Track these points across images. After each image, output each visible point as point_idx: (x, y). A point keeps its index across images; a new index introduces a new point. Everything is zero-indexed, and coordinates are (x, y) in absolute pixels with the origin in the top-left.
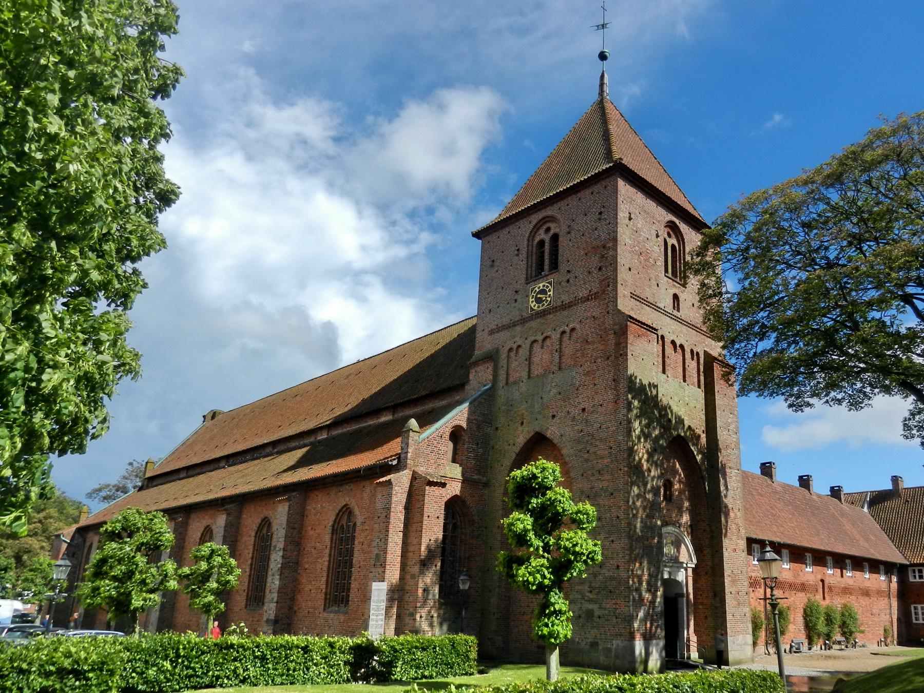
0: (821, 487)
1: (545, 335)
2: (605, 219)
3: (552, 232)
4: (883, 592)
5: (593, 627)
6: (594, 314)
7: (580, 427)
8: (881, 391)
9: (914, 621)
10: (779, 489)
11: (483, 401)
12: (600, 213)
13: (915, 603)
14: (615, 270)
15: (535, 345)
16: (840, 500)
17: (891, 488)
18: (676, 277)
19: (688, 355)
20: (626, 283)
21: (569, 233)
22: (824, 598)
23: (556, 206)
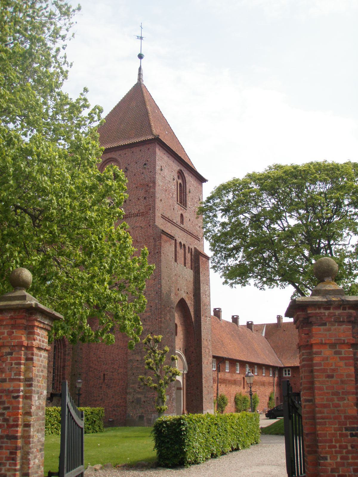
0: (242, 322)
2: (148, 169)
4: (271, 383)
5: (140, 407)
8: (289, 284)
12: (145, 164)
14: (154, 201)
16: (251, 329)
17: (276, 322)
19: (187, 251)
20: (160, 208)
22: (244, 388)
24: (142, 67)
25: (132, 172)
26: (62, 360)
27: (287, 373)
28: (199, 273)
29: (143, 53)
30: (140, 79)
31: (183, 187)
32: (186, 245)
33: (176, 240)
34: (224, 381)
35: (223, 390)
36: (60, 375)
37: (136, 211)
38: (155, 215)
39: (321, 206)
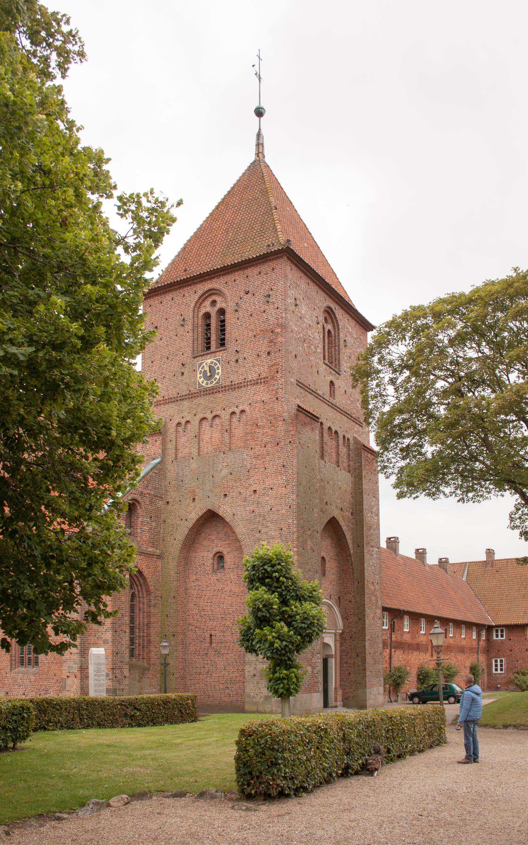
0: (432, 560)
1: (214, 413)
2: (273, 303)
4: (474, 648)
6: (264, 399)
9: (494, 672)
10: (401, 561)
11: (154, 475)
13: (496, 657)
15: (204, 422)
17: (485, 559)
18: (331, 363)
19: (341, 441)
21: (237, 311)
23: (223, 280)
24: (263, 132)
25: (247, 310)
26: (145, 614)
27: (499, 634)
28: (361, 479)
29: (263, 105)
31: (335, 337)
32: (339, 432)
33: (321, 423)
34: (401, 646)
35: (399, 658)
36: (143, 636)
37: (255, 376)
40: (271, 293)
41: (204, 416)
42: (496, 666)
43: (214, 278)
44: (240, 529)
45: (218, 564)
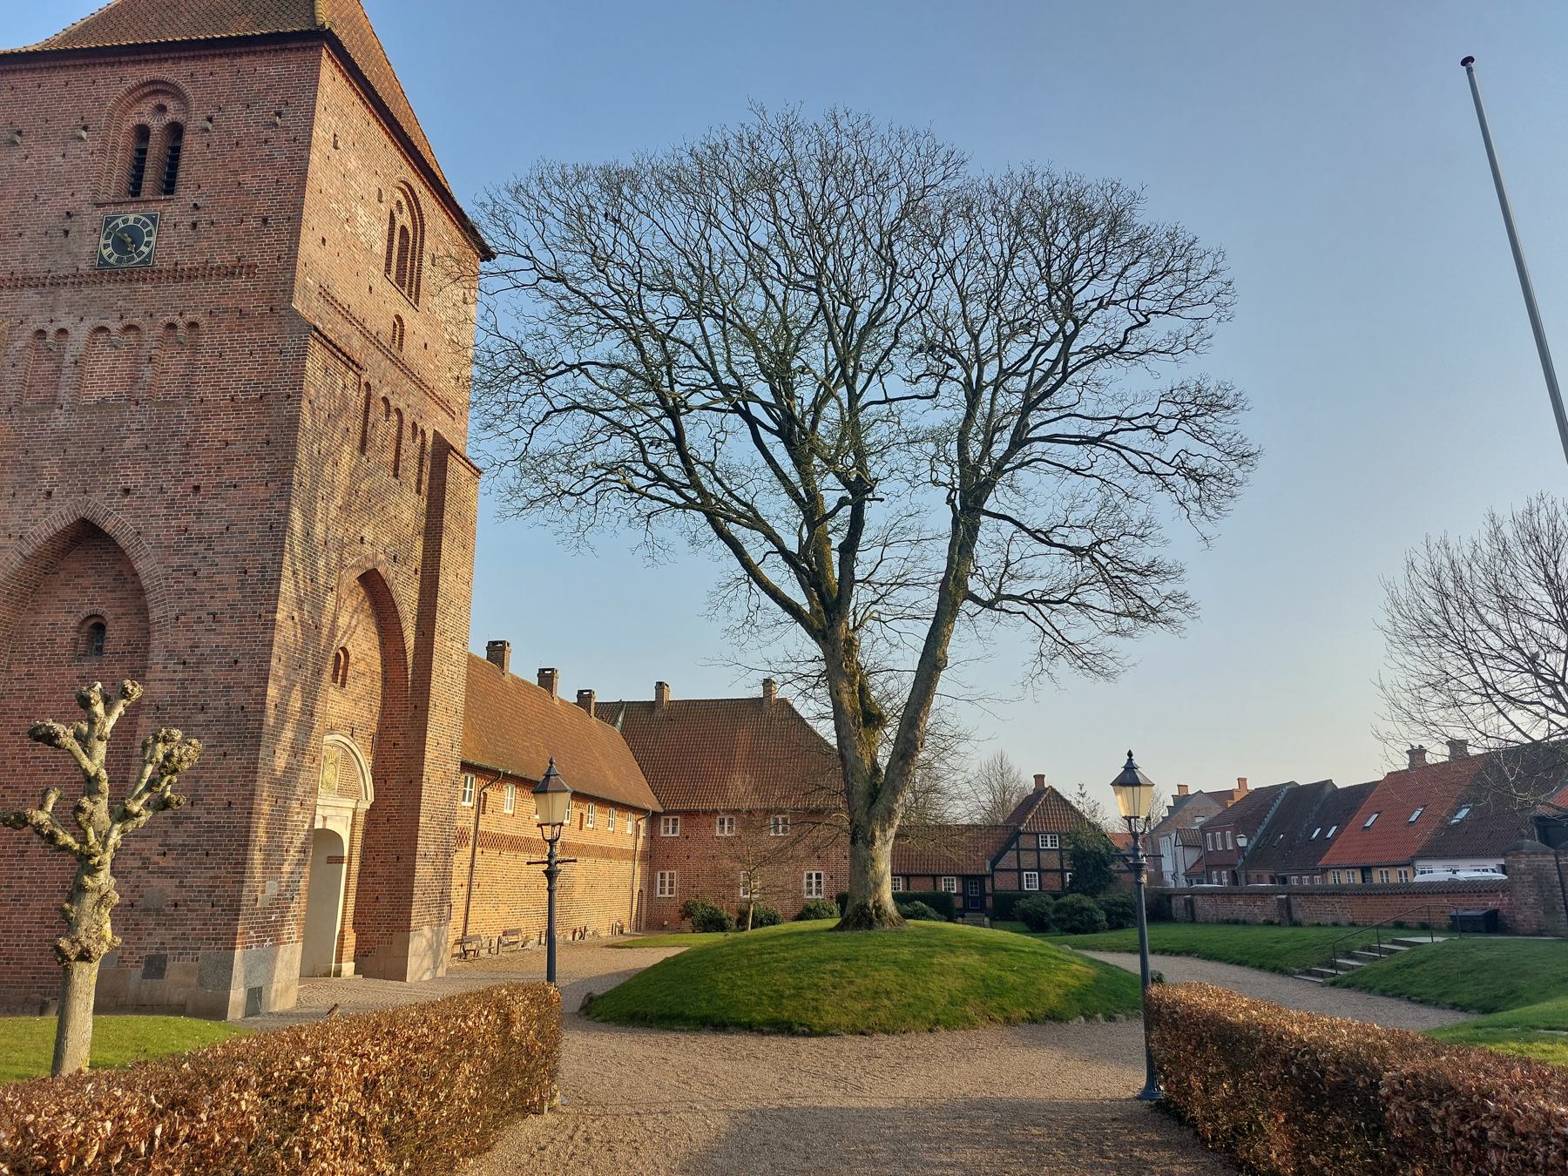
0: (566, 691)
1: (126, 321)
2: (287, 129)
3: (169, 117)
7: (183, 522)
23: (185, 68)
25: (229, 133)
30: (1130, 760)
38: (293, 279)
39: (1440, 1095)
40: (283, 109)
41: (103, 323)
42: (662, 883)
43: (166, 60)
44: (147, 566)
45: (90, 641)
